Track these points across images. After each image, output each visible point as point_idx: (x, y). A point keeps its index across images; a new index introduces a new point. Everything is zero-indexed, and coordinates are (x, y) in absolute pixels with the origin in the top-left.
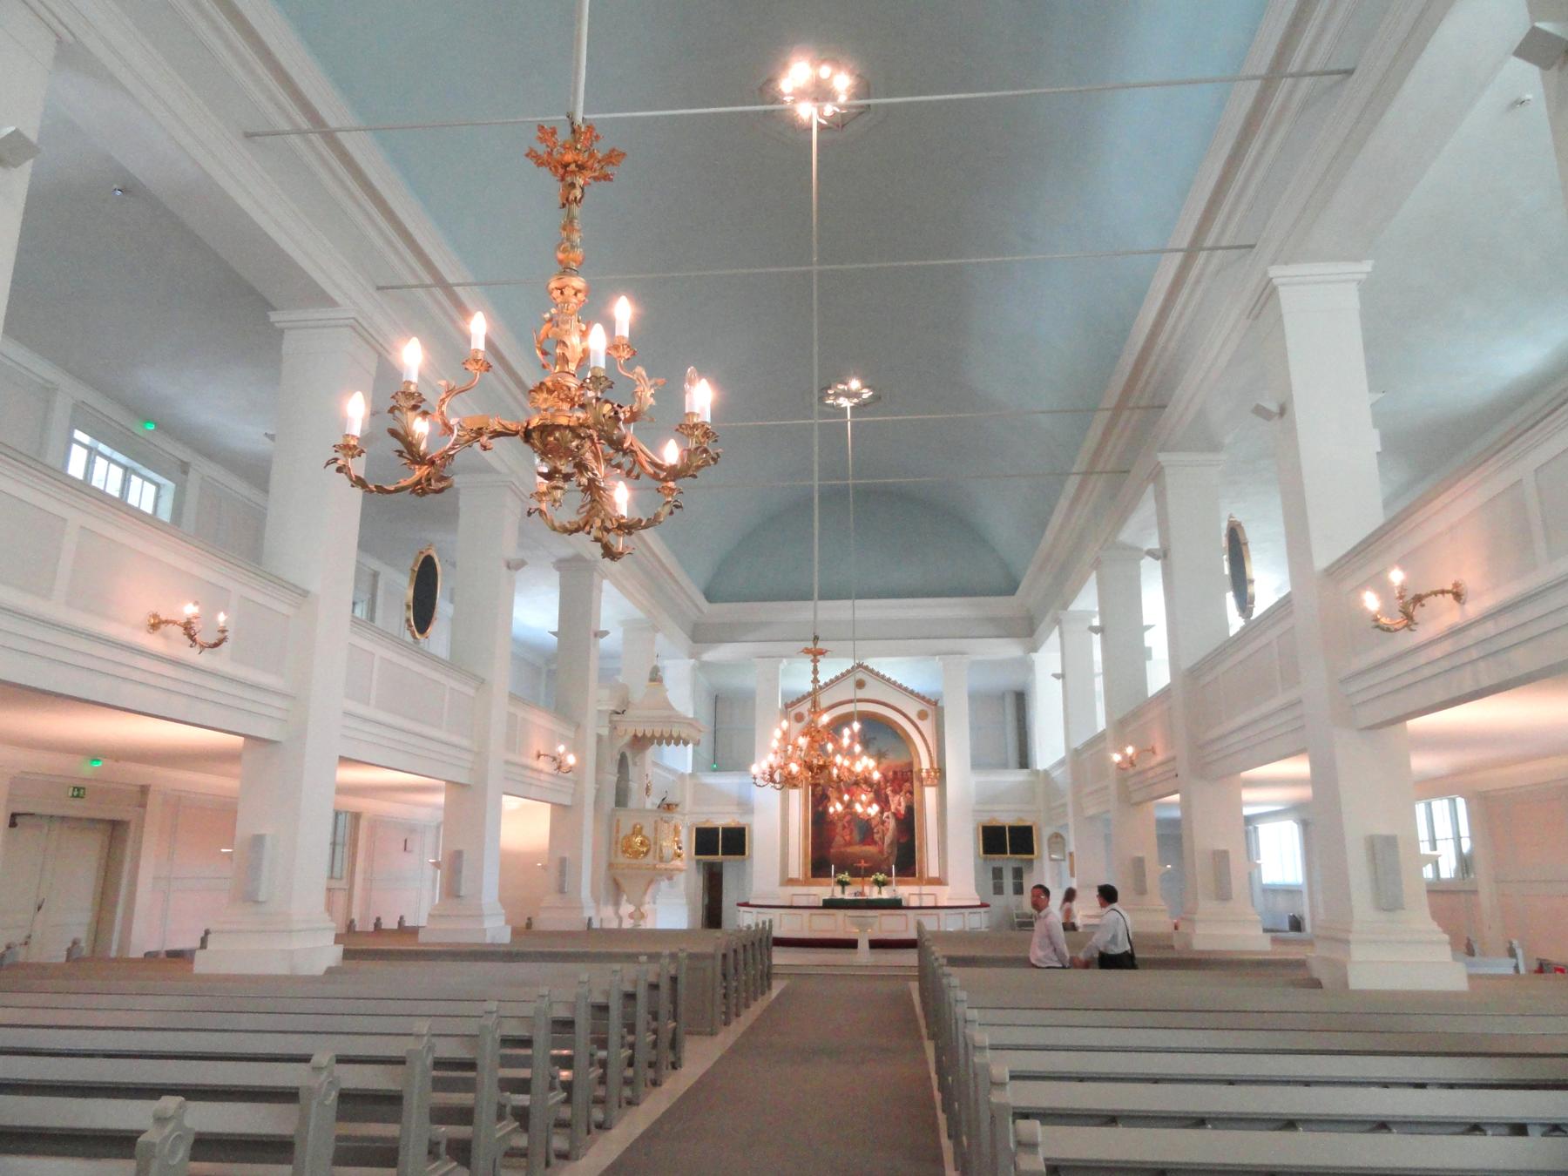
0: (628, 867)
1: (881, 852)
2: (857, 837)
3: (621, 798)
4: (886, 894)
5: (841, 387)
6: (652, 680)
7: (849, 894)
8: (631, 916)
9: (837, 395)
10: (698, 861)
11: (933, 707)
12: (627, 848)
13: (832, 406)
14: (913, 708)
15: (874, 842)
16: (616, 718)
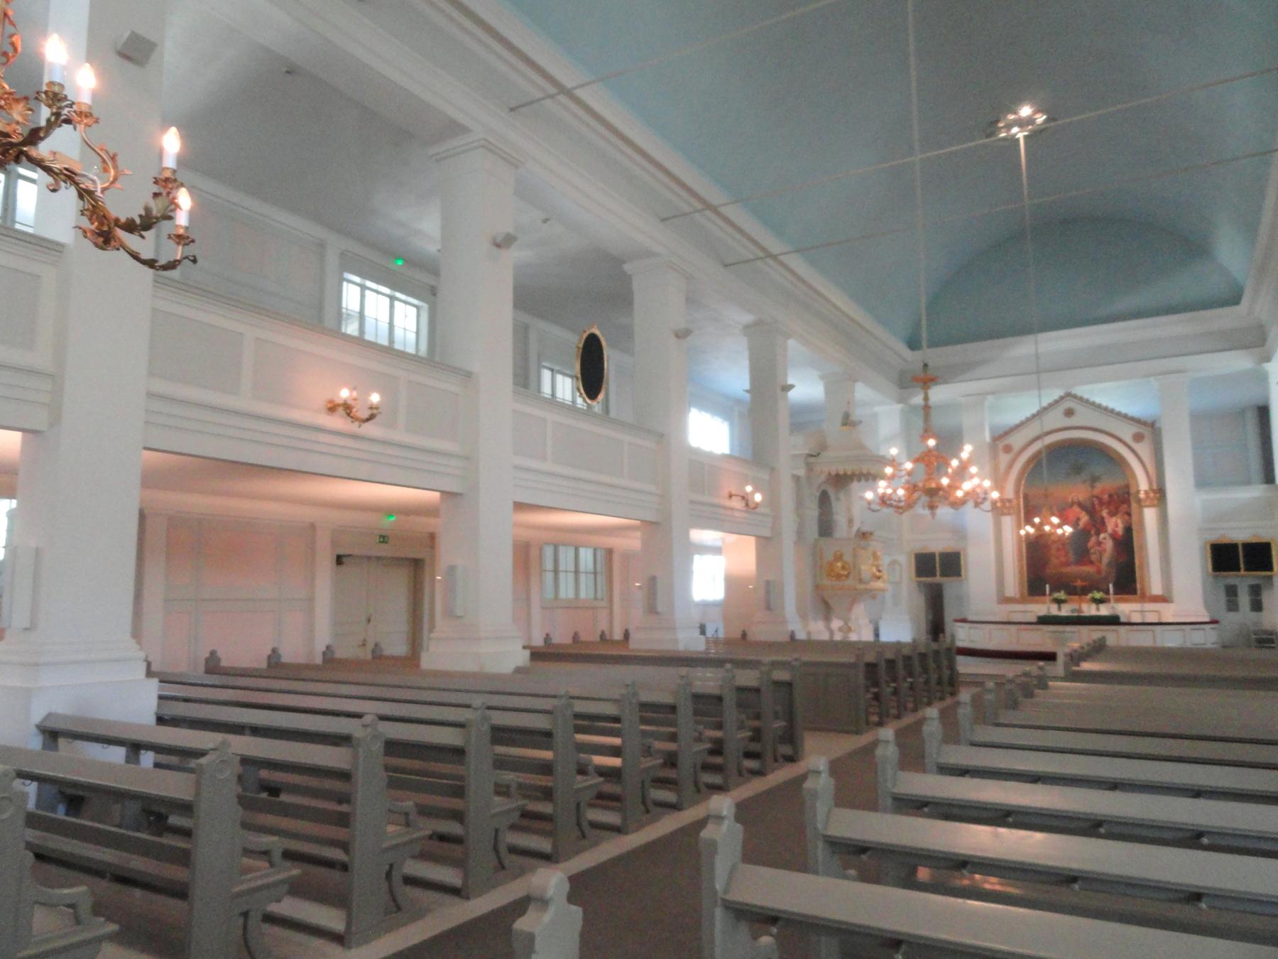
0: (833, 584)
1: (1099, 572)
2: (1072, 557)
3: (826, 528)
4: (1104, 611)
5: (1011, 117)
6: (844, 424)
7: (1065, 611)
8: (840, 629)
9: (1009, 127)
10: (919, 583)
11: (1149, 430)
12: (832, 573)
13: (1004, 139)
14: (1127, 432)
15: (1091, 563)
16: (812, 460)
